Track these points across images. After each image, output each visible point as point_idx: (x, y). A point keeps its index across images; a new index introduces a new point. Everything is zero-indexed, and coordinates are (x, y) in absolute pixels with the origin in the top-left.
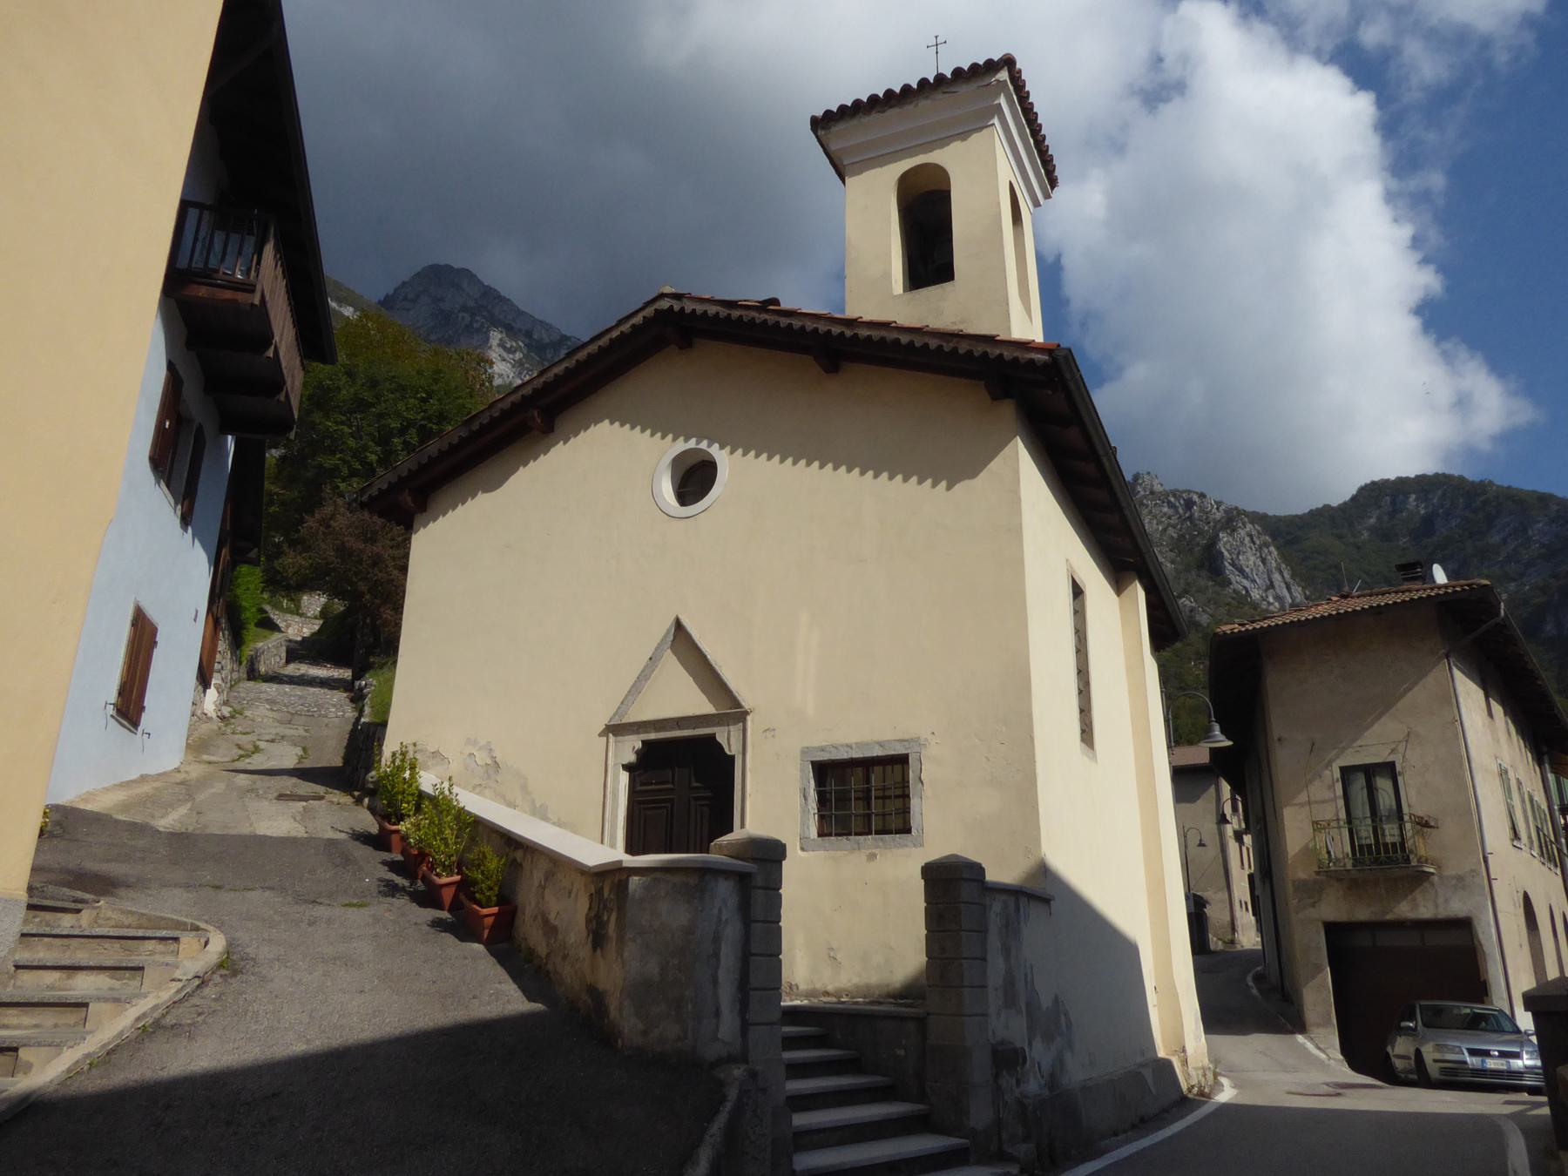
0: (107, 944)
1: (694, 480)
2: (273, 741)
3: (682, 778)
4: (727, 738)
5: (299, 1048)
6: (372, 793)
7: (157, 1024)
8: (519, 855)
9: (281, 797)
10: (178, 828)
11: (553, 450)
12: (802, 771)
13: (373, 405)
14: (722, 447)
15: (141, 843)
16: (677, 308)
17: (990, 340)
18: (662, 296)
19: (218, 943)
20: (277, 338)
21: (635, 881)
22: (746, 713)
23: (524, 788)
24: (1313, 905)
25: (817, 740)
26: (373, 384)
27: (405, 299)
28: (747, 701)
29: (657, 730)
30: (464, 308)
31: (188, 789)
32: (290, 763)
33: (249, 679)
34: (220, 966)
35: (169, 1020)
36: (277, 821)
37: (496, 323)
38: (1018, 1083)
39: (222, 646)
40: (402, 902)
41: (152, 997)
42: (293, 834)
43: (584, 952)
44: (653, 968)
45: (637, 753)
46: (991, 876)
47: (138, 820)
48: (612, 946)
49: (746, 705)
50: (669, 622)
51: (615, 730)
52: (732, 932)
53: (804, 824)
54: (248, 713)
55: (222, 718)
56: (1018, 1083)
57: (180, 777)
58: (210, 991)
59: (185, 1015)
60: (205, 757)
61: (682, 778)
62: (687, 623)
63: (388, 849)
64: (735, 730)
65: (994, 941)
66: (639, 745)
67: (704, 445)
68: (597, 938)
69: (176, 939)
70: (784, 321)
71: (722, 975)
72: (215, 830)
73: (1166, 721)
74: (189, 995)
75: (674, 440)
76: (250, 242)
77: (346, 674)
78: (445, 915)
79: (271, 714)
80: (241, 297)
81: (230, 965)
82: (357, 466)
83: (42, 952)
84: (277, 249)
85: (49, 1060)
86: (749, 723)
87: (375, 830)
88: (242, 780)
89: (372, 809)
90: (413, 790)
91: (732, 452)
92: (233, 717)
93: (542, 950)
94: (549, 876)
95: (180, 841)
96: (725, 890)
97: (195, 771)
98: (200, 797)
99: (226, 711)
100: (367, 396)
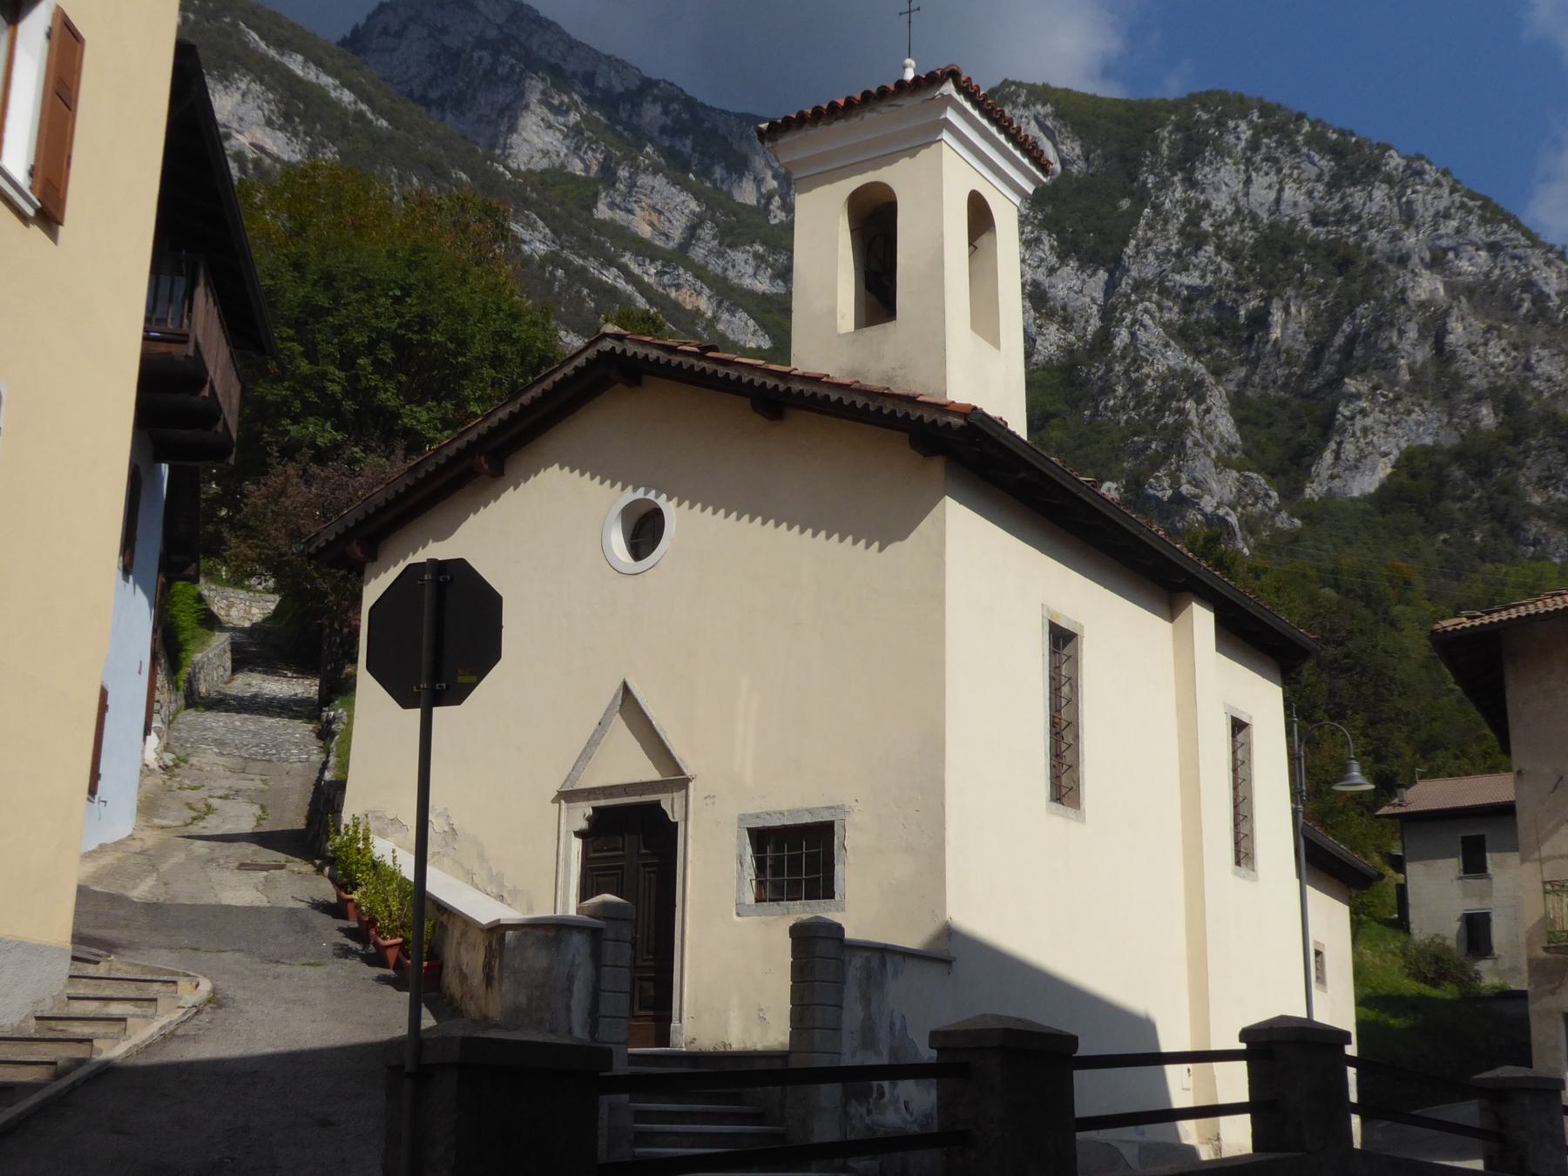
0: (126, 985)
1: (644, 531)
2: (226, 797)
3: (632, 841)
4: (670, 804)
5: (270, 1050)
6: (332, 861)
7: (172, 1034)
8: (444, 919)
9: (243, 866)
10: (151, 898)
11: (503, 496)
12: (739, 837)
13: (329, 312)
14: (669, 499)
15: (121, 912)
16: (618, 350)
17: (911, 400)
18: (606, 335)
19: (206, 986)
20: (211, 373)
21: (509, 934)
22: (688, 780)
23: (481, 856)
24: (1552, 992)
25: (753, 809)
26: (328, 280)
27: (385, 32)
28: (689, 766)
29: (606, 797)
30: (481, 43)
31: (151, 859)
32: (247, 826)
33: (188, 706)
34: (209, 1001)
35: (179, 1032)
36: (240, 891)
37: (533, 64)
38: (869, 1112)
39: (161, 679)
40: (355, 964)
41: (166, 1017)
42: (257, 904)
43: (482, 991)
44: (522, 999)
45: (589, 819)
46: (850, 934)
47: (113, 890)
48: (496, 984)
49: (688, 772)
50: (618, 685)
51: (567, 796)
52: (583, 974)
53: (740, 890)
54: (194, 760)
55: (165, 768)
56: (869, 1112)
57: (137, 846)
58: (204, 1017)
59: (188, 1029)
60: (157, 821)
61: (632, 841)
62: (631, 686)
63: (345, 917)
64: (678, 796)
65: (852, 993)
66: (590, 812)
67: (651, 496)
68: (489, 980)
69: (175, 983)
70: (722, 371)
71: (574, 1004)
72: (184, 900)
73: (1293, 758)
74: (190, 1019)
75: (623, 488)
76: (181, 283)
77: (306, 688)
78: (390, 972)
79: (219, 760)
80: (175, 349)
81: (216, 1001)
82: (312, 397)
83: (82, 989)
84: (207, 284)
85: (112, 1048)
86: (691, 790)
87: (334, 900)
88: (200, 847)
89: (332, 878)
90: (366, 860)
91: (679, 505)
92: (176, 766)
93: (458, 995)
94: (464, 934)
95: (153, 910)
96: (578, 941)
97: (151, 838)
98: (164, 867)
99: (168, 758)
100: (323, 300)
